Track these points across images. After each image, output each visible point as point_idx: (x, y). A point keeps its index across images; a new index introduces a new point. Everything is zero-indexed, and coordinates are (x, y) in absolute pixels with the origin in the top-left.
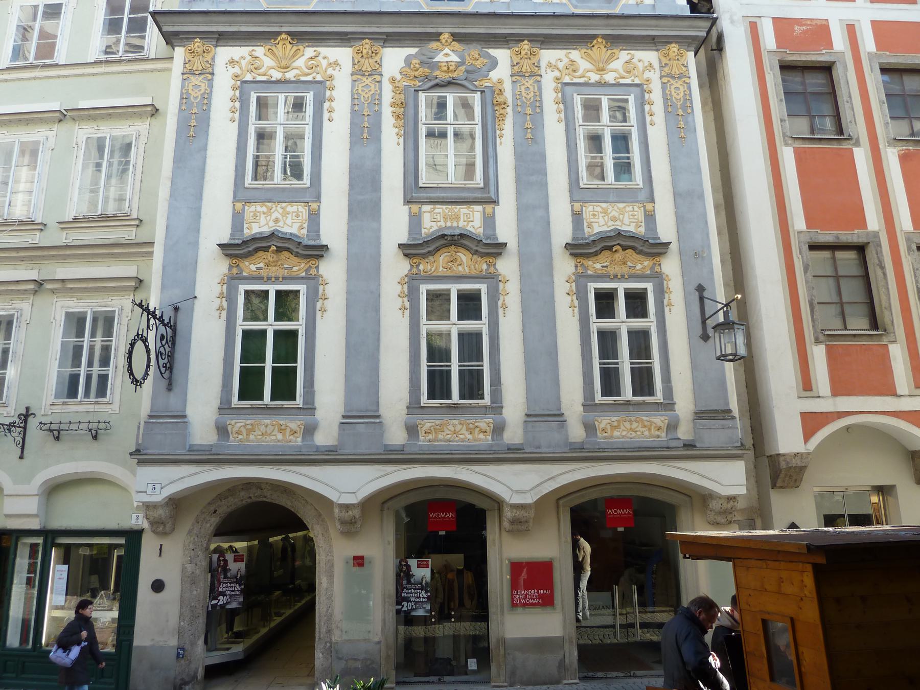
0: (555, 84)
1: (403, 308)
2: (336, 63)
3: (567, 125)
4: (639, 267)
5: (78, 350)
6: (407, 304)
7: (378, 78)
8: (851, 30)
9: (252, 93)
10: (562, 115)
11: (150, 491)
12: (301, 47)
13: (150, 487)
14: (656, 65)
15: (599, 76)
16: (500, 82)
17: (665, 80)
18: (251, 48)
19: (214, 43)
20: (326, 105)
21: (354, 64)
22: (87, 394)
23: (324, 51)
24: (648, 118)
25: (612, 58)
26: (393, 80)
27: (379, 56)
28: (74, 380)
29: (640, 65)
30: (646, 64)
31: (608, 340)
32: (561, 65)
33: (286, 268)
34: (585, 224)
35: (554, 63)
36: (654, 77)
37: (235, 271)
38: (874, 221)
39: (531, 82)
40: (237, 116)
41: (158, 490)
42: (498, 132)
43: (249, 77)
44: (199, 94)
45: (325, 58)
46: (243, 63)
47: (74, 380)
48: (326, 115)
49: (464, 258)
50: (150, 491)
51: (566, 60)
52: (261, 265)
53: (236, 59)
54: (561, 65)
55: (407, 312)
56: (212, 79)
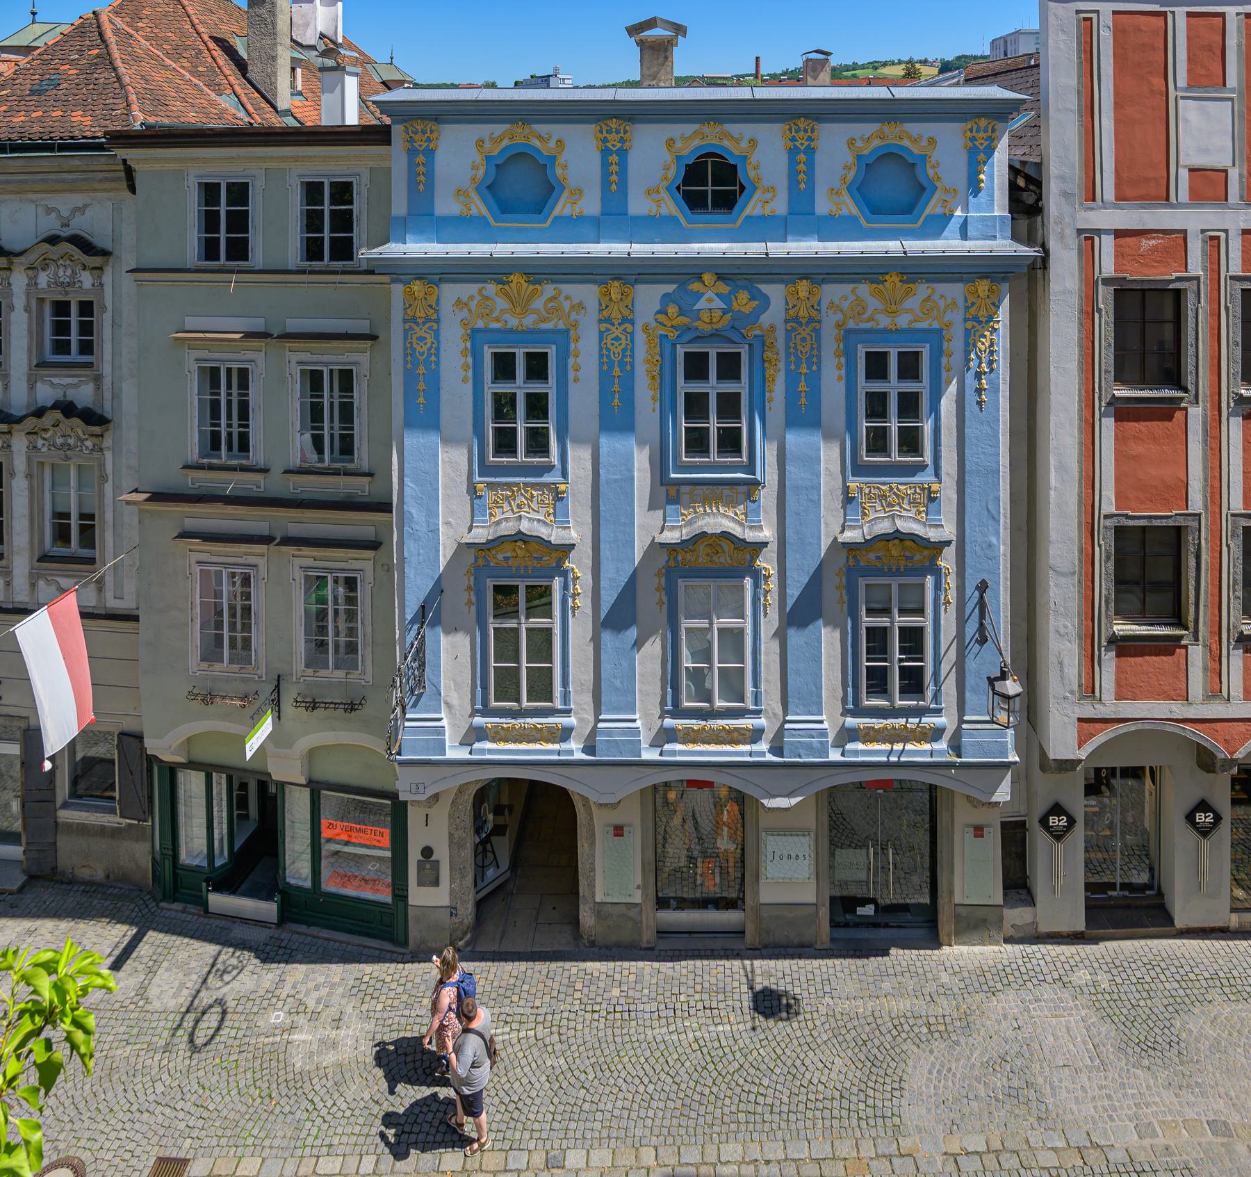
0: (836, 331)
1: (661, 603)
2: (580, 306)
3: (847, 381)
4: (917, 557)
5: (215, 405)
6: (665, 599)
7: (629, 328)
8: (1214, 242)
9: (486, 347)
10: (843, 372)
11: (414, 791)
13: (414, 786)
14: (961, 303)
15: (889, 320)
16: (773, 328)
17: (969, 325)
20: (571, 361)
21: (601, 310)
22: (230, 448)
23: (567, 289)
25: (908, 293)
26: (646, 328)
28: (215, 437)
29: (942, 303)
30: (949, 301)
32: (846, 305)
36: (956, 317)
37: (481, 562)
38: (1197, 502)
39: (808, 330)
40: (470, 373)
41: (421, 790)
42: (767, 395)
43: (480, 324)
44: (425, 349)
45: (567, 298)
46: (473, 304)
47: (215, 437)
48: (571, 375)
49: (726, 548)
50: (414, 791)
51: (851, 298)
53: (465, 299)
54: (846, 305)
55: (665, 607)
56: (438, 329)
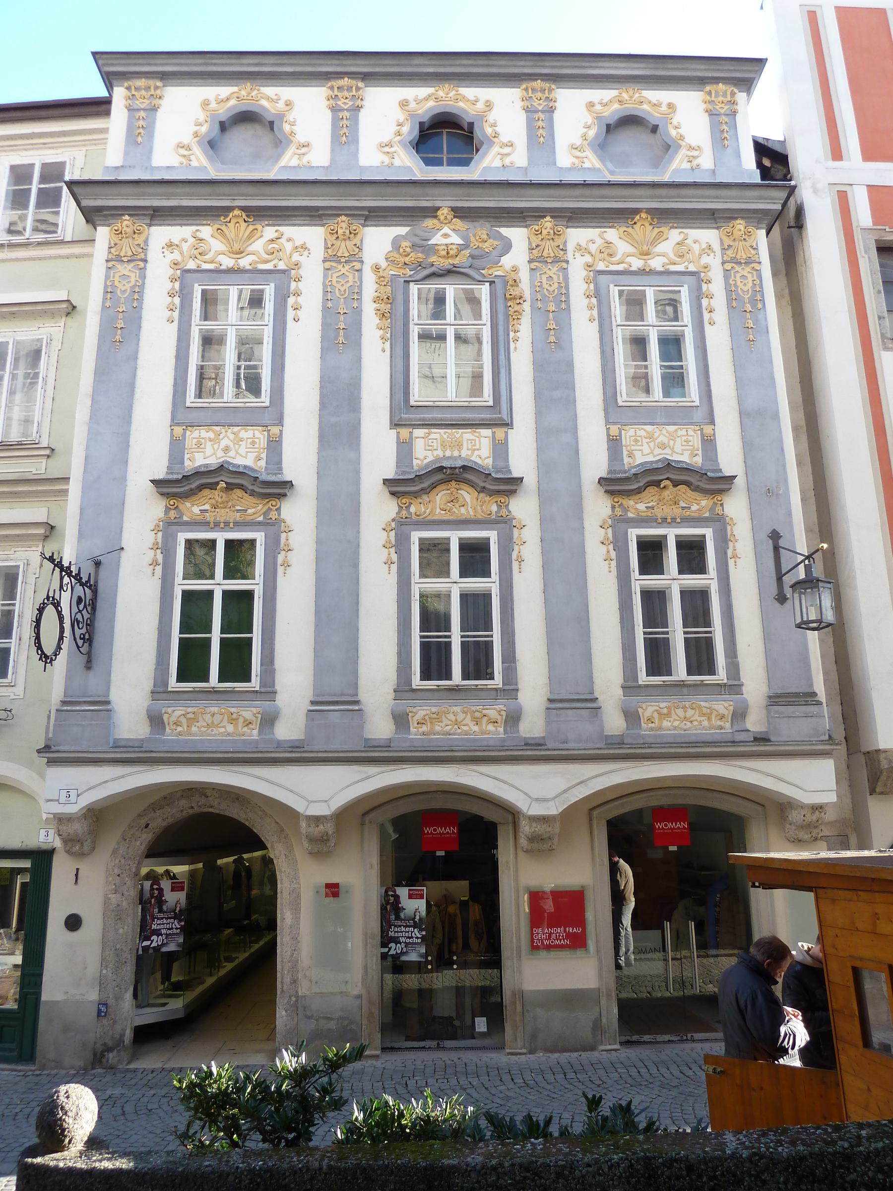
12: (259, 227)
18: (195, 228)
19: (148, 221)
24: (706, 316)
27: (359, 237)
30: (704, 246)
31: (654, 602)
33: (238, 511)
34: (625, 453)
35: (584, 245)
45: (289, 240)
49: (468, 497)
51: (599, 242)
52: (207, 507)
